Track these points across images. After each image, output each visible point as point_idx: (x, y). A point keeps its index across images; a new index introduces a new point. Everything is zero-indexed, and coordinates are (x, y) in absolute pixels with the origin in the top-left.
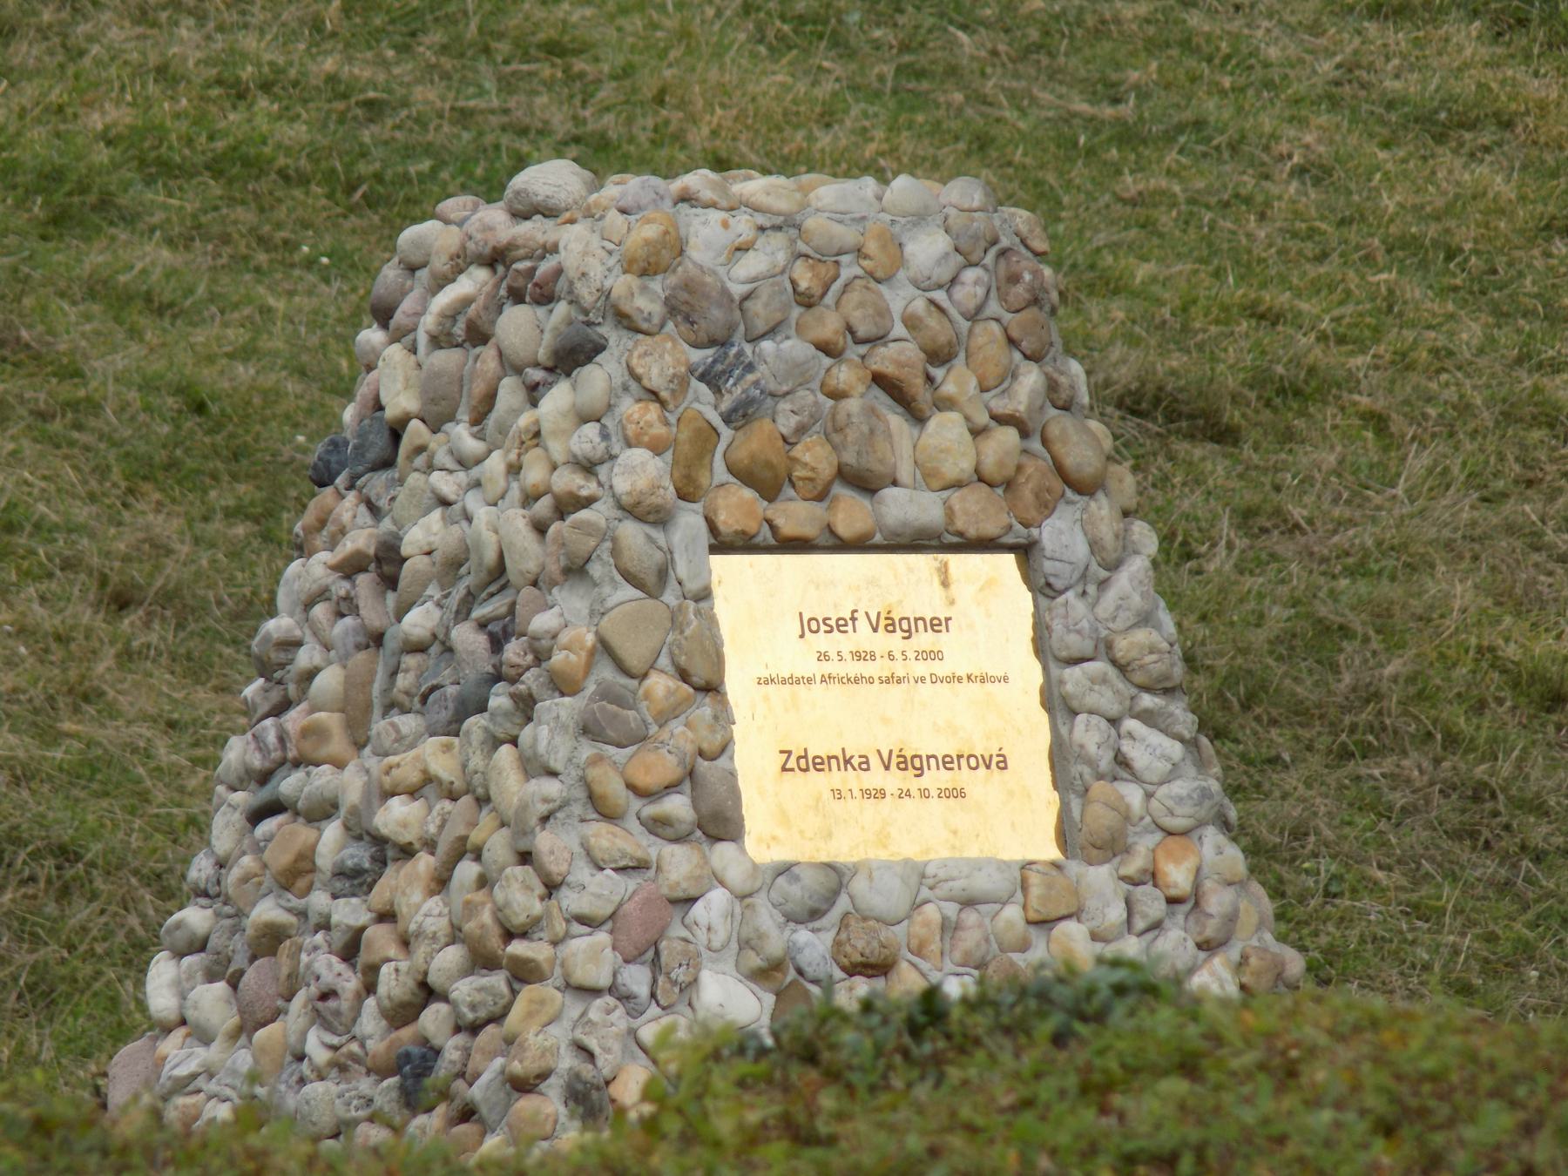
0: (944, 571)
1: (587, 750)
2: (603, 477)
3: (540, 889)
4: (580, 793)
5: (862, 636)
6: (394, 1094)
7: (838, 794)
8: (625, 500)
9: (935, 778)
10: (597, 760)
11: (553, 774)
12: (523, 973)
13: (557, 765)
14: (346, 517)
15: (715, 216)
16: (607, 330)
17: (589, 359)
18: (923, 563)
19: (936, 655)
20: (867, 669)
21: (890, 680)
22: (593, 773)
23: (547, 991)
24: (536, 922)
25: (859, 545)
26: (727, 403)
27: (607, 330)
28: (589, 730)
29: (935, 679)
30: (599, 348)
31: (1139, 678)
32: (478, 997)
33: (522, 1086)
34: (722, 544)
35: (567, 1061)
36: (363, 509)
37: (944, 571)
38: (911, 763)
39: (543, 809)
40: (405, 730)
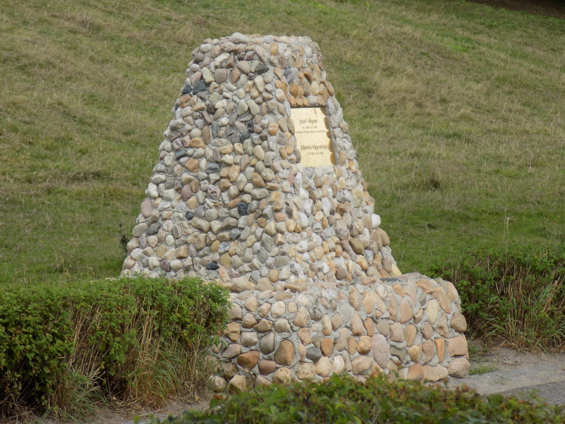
0: (315, 111)
1: (279, 146)
2: (274, 94)
3: (273, 173)
4: (279, 155)
5: (307, 124)
6: (237, 212)
7: (308, 154)
8: (279, 98)
9: (320, 150)
10: (281, 148)
11: (272, 151)
12: (271, 189)
13: (274, 149)
14: (195, 100)
15: (282, 44)
16: (269, 66)
17: (266, 71)
18: (312, 109)
19: (316, 127)
20: (309, 130)
21: (312, 132)
22: (282, 151)
23: (279, 192)
24: (273, 179)
25: (304, 106)
26: (288, 80)
27: (269, 66)
28: (279, 142)
29: (318, 132)
30: (268, 69)
31: (344, 131)
32: (261, 194)
33: (277, 211)
34: (292, 107)
35: (285, 206)
36: (199, 99)
37: (315, 111)
38: (316, 148)
39: (273, 157)
40: (223, 141)
